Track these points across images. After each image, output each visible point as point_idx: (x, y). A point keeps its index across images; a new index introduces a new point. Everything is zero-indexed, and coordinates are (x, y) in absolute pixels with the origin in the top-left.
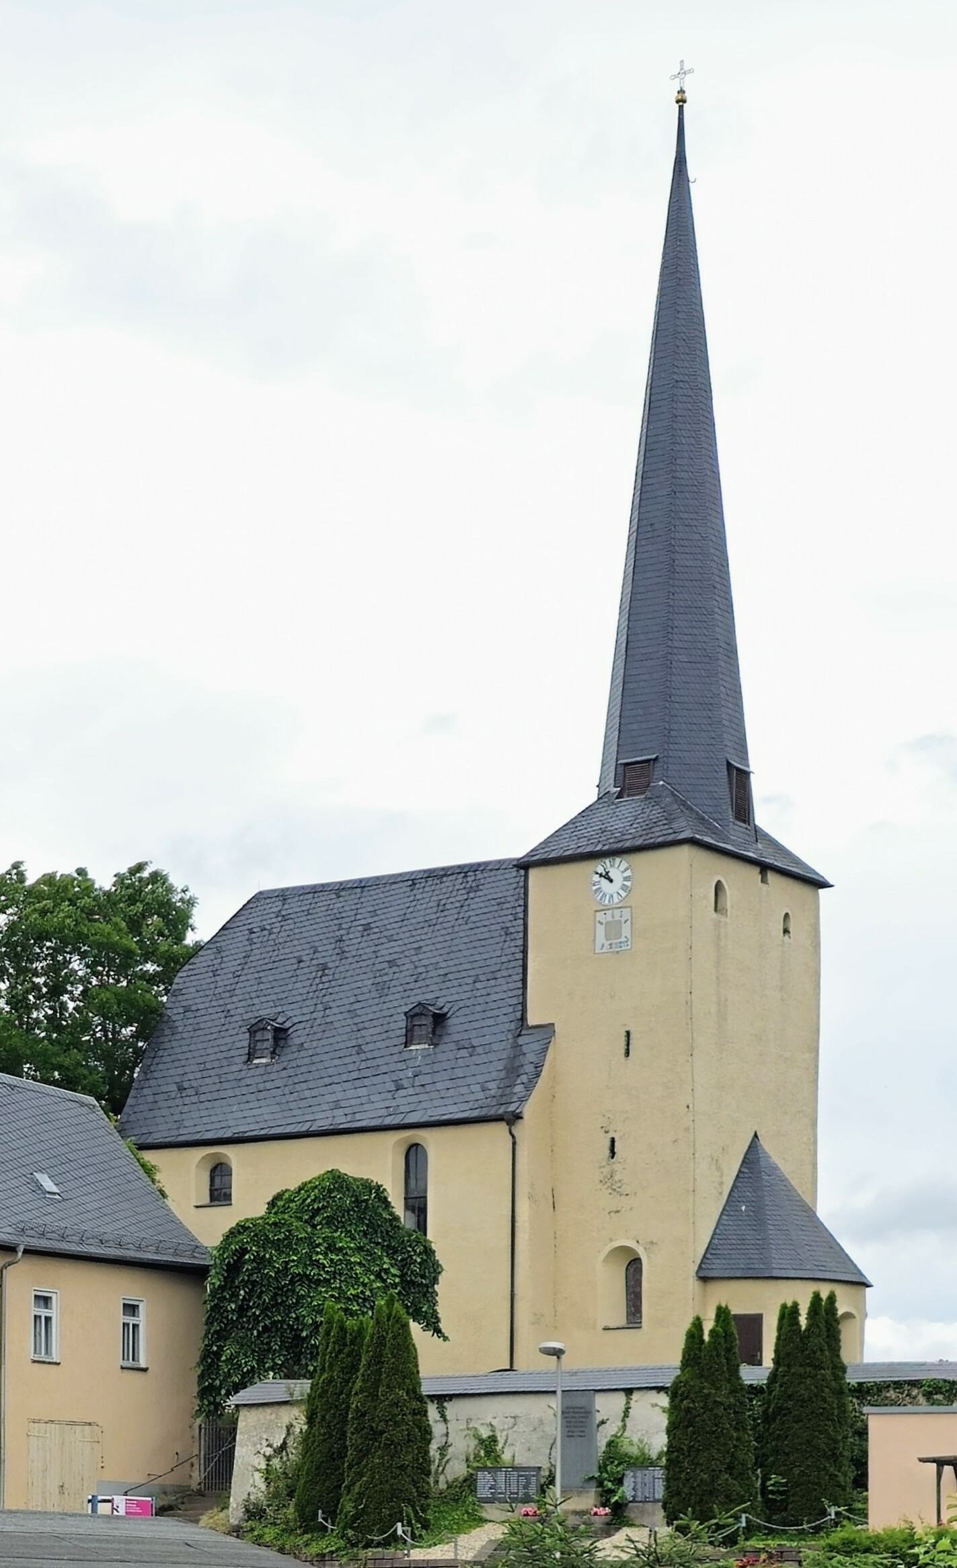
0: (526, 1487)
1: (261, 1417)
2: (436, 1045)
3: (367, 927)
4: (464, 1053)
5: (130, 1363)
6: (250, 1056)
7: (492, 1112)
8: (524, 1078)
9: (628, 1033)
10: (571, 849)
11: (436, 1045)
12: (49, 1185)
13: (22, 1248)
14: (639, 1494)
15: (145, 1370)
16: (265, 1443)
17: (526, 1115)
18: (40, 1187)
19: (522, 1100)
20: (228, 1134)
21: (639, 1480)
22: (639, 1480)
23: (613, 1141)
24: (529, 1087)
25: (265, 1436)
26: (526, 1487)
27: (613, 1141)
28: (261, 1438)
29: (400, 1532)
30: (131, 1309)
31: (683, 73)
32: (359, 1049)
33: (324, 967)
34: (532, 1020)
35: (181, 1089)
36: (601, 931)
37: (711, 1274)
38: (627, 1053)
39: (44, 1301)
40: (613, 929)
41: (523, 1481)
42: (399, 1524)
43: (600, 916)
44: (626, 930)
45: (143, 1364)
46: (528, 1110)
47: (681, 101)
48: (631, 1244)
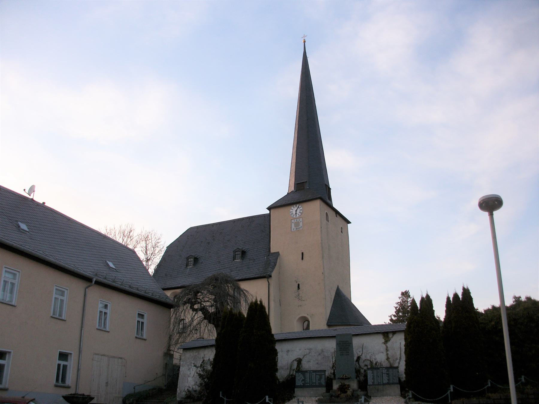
0: (320, 379)
1: (192, 354)
2: (243, 260)
3: (221, 233)
4: (251, 261)
5: (140, 336)
6: (187, 265)
7: (262, 275)
8: (271, 266)
9: (303, 254)
10: (284, 203)
11: (243, 260)
12: (111, 265)
13: (94, 280)
14: (376, 381)
15: (145, 340)
16: (193, 365)
17: (272, 276)
18: (108, 265)
19: (272, 271)
20: (180, 285)
21: (375, 375)
22: (375, 375)
23: (299, 285)
24: (273, 268)
25: (193, 362)
26: (320, 379)
27: (299, 285)
28: (191, 363)
29: (267, 401)
30: (141, 316)
31: (304, 36)
32: (219, 262)
33: (209, 243)
34: (272, 251)
35: (166, 275)
36: (293, 225)
37: (332, 324)
38: (302, 259)
39: (106, 306)
40: (297, 224)
41: (318, 377)
42: (267, 397)
43: (293, 221)
44: (301, 224)
45: (144, 337)
46: (273, 274)
47: (305, 42)
48: (306, 315)
